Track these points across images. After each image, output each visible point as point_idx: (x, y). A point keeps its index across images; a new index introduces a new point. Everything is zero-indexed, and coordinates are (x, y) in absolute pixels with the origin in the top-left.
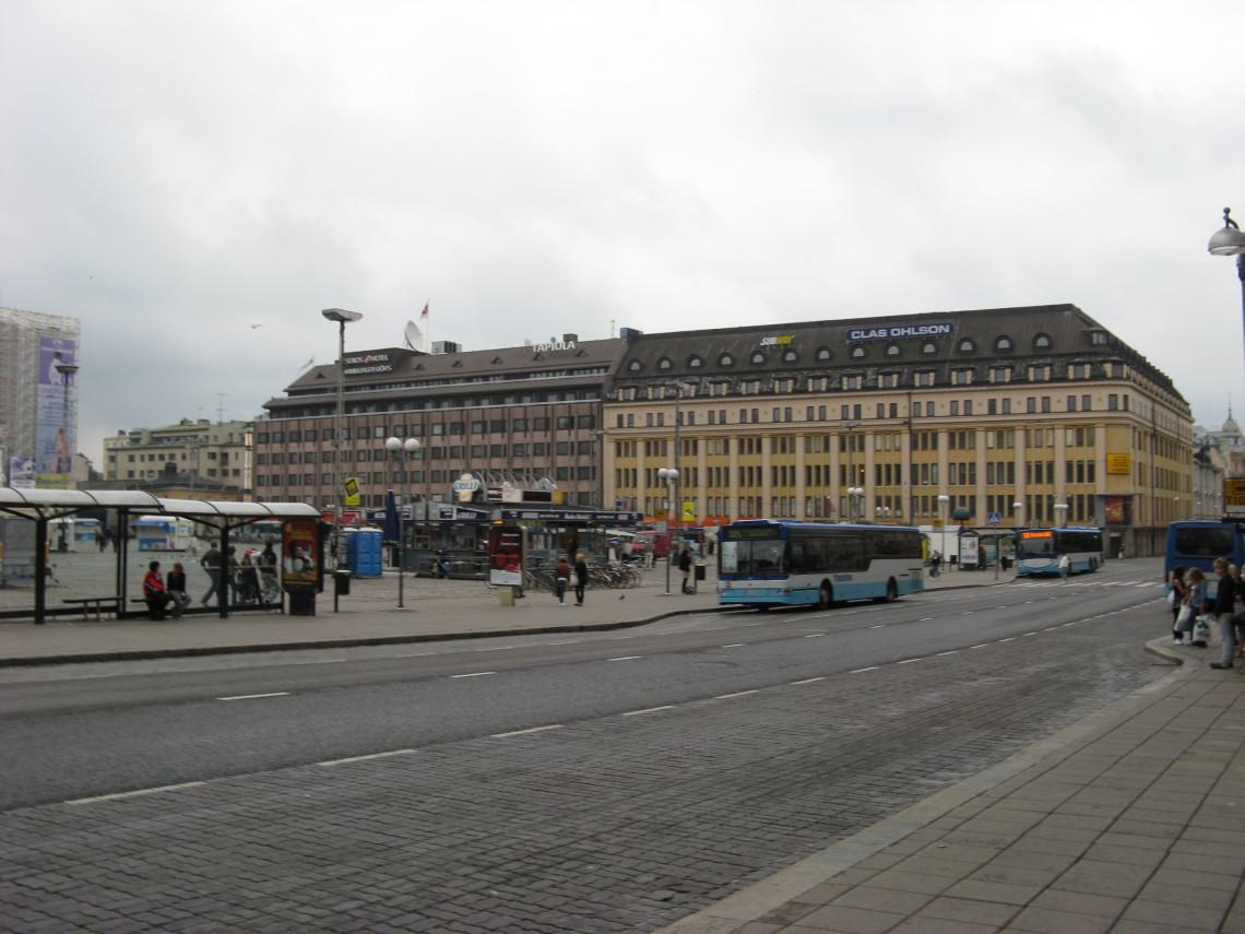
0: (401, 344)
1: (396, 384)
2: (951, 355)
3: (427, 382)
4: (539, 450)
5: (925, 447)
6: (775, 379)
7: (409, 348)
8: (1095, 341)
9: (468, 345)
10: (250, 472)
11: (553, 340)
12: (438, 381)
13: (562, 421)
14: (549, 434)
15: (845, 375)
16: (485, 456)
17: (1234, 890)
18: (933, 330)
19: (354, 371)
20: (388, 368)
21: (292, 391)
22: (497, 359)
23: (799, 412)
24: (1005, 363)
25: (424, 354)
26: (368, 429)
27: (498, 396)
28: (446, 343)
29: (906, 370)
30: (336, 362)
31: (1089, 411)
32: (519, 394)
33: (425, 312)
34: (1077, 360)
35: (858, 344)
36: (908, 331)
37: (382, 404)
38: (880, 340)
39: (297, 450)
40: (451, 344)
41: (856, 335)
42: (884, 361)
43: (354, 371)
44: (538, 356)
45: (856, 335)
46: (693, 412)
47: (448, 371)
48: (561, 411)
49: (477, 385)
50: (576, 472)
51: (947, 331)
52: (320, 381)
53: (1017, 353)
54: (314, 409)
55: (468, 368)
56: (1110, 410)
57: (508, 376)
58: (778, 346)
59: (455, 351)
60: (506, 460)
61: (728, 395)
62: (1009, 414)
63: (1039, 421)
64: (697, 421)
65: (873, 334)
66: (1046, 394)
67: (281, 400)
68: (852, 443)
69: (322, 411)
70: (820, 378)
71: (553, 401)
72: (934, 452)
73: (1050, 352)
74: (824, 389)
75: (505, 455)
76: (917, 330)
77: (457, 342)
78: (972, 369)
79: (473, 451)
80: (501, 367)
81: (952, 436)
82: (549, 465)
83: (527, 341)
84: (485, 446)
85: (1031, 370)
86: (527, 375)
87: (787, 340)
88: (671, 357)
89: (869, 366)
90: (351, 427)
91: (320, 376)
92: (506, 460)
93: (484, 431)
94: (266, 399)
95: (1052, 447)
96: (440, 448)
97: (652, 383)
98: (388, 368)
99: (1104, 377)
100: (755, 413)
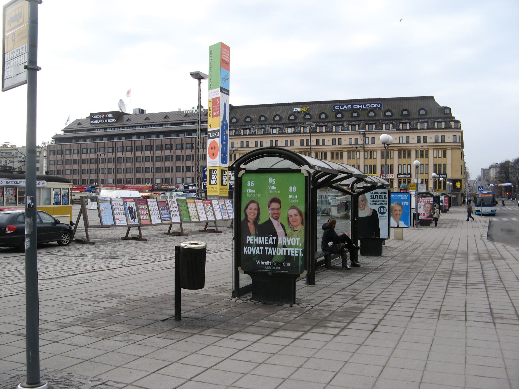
0: (117, 109)
1: (117, 127)
2: (381, 117)
3: (132, 127)
4: (148, 159)
5: (404, 157)
6: (301, 127)
7: (120, 111)
8: (446, 112)
9: (149, 111)
10: (46, 168)
11: (193, 108)
12: (157, 125)
13: (128, 148)
14: (133, 153)
15: (334, 125)
16: (143, 161)
17: (445, 299)
18: (373, 106)
19: (97, 122)
20: (114, 120)
21: (65, 131)
22: (147, 118)
23: (431, 138)
24: (406, 121)
25: (129, 114)
26: (123, 147)
27: (168, 134)
28: (139, 109)
29: (361, 123)
30: (87, 118)
31: (374, 144)
32: (178, 132)
33: (128, 93)
34: (439, 120)
35: (338, 112)
36: (361, 106)
37: (111, 137)
38: (348, 110)
39: (69, 158)
40: (141, 110)
41: (337, 107)
42: (351, 119)
43: (97, 122)
44: (186, 115)
45: (337, 107)
46: (325, 139)
47: (142, 121)
48: (84, 146)
49: (137, 130)
50: (164, 169)
51: (379, 106)
52: (79, 126)
53: (411, 117)
54: (77, 139)
55: (152, 121)
56: (453, 142)
57: (172, 124)
58: (301, 112)
59: (143, 113)
60: (172, 163)
61: (279, 134)
62: (444, 142)
63: (422, 146)
64: (429, 140)
65: (345, 107)
66: (443, 134)
67: (60, 135)
68: (404, 154)
69: (74, 140)
70: (322, 126)
71: (174, 137)
72: (409, 159)
73: (426, 117)
74: (324, 131)
75: (172, 160)
76: (365, 106)
77: (144, 109)
78: (392, 123)
79: (118, 160)
80: (188, 118)
81: (332, 154)
82: (152, 166)
83: (179, 109)
84: (124, 158)
85: (419, 124)
86: (181, 124)
87: (305, 109)
88: (311, 113)
89: (344, 121)
90: (96, 147)
91: (79, 124)
92: (172, 163)
93: (54, 154)
94: (53, 134)
95: (359, 159)
96: (77, 160)
97: (243, 128)
98: (114, 120)
99: (451, 127)
100: (324, 140)
